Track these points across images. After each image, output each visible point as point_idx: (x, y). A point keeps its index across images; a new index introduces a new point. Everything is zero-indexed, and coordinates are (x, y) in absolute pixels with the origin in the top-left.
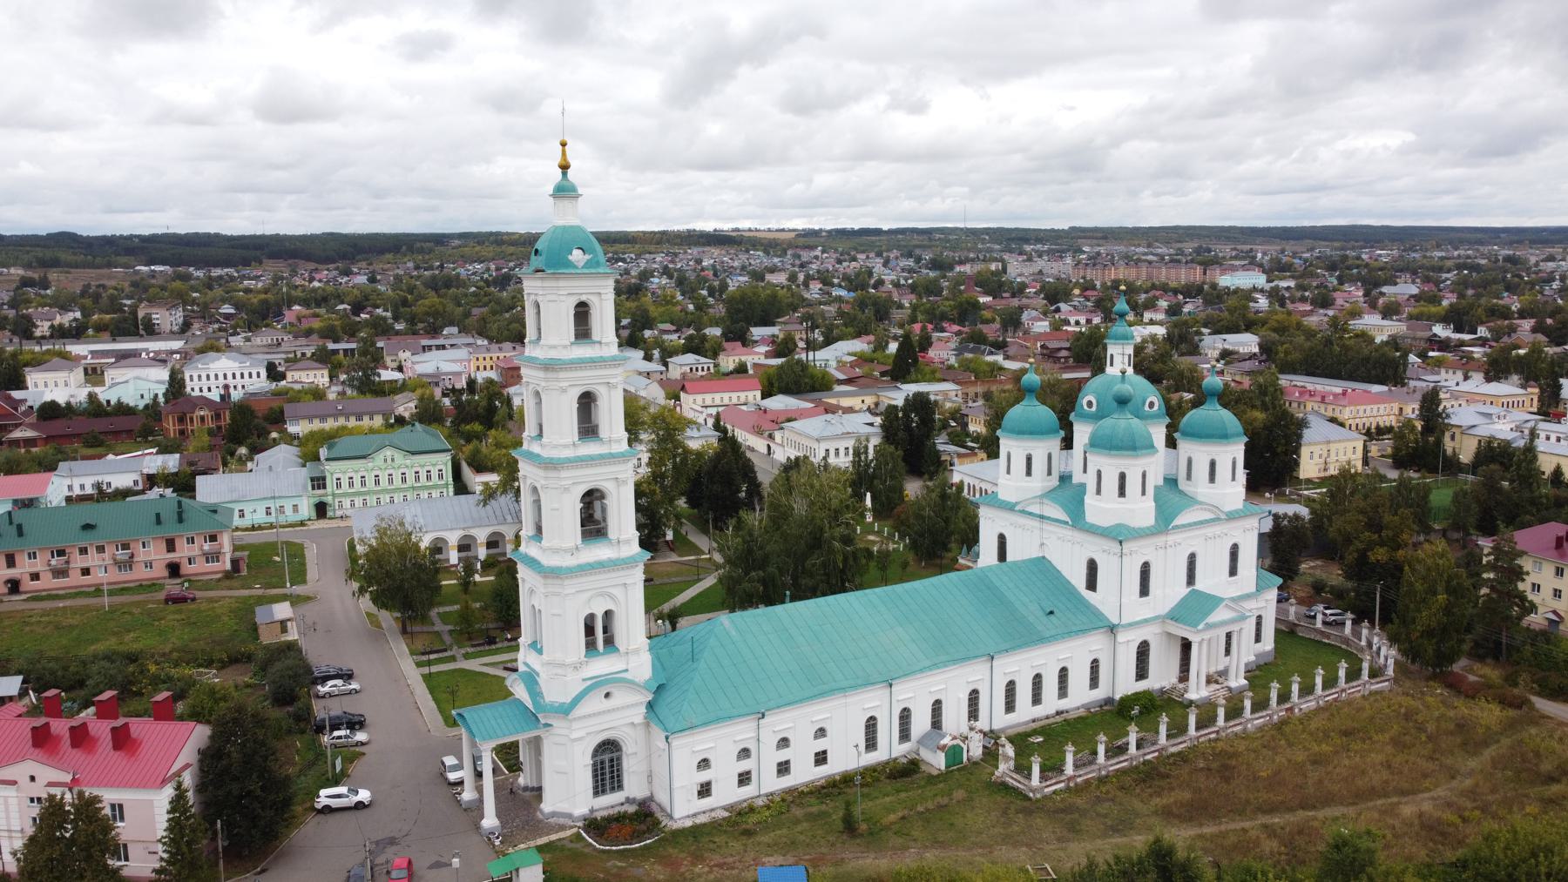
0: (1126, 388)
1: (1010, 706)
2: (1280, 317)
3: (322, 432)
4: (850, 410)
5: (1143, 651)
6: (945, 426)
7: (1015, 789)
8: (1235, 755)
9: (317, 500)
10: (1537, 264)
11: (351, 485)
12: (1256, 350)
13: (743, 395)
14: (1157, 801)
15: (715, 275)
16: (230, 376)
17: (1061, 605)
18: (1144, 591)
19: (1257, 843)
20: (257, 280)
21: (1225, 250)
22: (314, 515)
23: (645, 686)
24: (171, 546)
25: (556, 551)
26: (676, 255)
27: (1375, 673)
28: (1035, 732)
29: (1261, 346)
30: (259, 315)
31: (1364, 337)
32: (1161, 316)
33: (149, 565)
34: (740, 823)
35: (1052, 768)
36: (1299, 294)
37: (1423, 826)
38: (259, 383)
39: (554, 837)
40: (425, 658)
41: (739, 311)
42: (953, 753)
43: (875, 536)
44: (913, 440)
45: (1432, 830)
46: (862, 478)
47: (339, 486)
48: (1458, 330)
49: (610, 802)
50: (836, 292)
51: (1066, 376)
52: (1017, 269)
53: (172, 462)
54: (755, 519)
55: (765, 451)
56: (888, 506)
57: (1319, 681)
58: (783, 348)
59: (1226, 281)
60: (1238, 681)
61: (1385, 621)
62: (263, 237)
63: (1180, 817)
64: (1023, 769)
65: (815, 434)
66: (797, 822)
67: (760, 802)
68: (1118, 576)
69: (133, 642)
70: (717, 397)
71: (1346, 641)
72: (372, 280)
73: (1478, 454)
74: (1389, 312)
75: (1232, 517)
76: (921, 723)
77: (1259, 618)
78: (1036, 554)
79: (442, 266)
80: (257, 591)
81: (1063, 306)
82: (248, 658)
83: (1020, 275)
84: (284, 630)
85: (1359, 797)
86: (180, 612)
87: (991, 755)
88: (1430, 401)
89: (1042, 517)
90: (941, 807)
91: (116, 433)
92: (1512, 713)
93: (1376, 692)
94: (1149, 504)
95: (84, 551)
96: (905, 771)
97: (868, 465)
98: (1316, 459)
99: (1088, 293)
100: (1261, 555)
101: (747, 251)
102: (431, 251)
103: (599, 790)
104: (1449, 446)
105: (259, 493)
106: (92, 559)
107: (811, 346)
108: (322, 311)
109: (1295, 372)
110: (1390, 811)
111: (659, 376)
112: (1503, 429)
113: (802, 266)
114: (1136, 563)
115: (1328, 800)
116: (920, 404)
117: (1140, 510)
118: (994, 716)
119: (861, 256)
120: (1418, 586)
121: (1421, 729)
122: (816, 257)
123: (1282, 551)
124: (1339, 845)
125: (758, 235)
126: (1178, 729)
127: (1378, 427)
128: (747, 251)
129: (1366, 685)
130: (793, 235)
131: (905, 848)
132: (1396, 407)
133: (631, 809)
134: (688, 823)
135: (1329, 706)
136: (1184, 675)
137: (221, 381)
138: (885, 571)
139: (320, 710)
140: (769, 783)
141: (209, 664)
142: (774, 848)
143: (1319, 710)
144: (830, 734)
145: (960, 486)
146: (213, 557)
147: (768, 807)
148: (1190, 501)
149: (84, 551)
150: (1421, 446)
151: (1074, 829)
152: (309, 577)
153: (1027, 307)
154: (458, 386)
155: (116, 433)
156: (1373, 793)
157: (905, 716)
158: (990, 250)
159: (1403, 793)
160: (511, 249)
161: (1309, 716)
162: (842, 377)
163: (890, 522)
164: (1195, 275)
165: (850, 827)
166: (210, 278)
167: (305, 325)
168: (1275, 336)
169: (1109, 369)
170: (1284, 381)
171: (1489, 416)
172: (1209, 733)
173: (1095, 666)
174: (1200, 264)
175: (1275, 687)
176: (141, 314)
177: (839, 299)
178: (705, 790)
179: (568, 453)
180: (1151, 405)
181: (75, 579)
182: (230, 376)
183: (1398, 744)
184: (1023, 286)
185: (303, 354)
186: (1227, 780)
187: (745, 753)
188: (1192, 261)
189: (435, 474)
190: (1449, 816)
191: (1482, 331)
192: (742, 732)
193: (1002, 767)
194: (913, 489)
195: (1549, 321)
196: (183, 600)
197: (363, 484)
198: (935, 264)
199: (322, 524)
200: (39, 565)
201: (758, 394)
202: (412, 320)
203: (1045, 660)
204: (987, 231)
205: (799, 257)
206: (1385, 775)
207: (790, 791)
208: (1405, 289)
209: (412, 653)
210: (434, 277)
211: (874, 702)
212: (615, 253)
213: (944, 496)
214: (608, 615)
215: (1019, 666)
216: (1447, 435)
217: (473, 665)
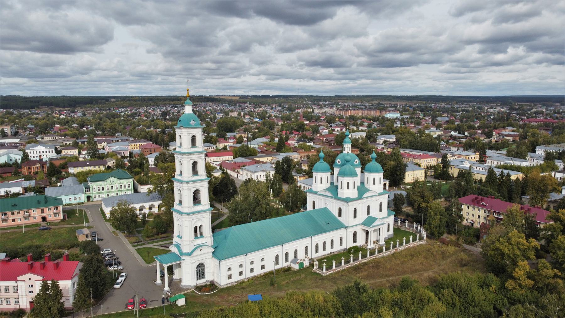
0: (348, 158)
1: (317, 251)
2: (403, 129)
3: (83, 172)
4: (263, 162)
5: (355, 234)
6: (294, 167)
7: (319, 274)
8: (379, 262)
9: (87, 195)
10: (487, 110)
12: (395, 140)
15: (211, 113)
16: (41, 152)
18: (355, 217)
20: (39, 114)
21: (387, 104)
22: (86, 200)
23: (212, 247)
24: (43, 211)
26: (196, 105)
27: (421, 239)
28: (324, 258)
29: (396, 139)
30: (45, 129)
31: (429, 136)
32: (365, 128)
34: (240, 286)
35: (329, 267)
36: (410, 120)
38: (53, 155)
39: (186, 292)
41: (222, 127)
43: (276, 204)
44: (285, 171)
46: (270, 184)
47: (95, 190)
48: (459, 133)
49: (201, 282)
51: (333, 150)
52: (318, 111)
53: (32, 183)
54: (238, 198)
55: (236, 176)
56: (277, 194)
57: (404, 241)
58: (240, 141)
59: (388, 116)
60: (382, 242)
62: (37, 97)
64: (321, 268)
66: (257, 285)
68: (348, 210)
69: (36, 242)
70: (218, 158)
72: (84, 115)
73: (459, 174)
74: (438, 127)
75: (380, 194)
76: (291, 257)
77: (389, 224)
79: (109, 109)
80: (73, 225)
81: (333, 125)
86: (49, 232)
87: (312, 265)
88: (444, 157)
89: (325, 196)
90: (298, 279)
92: (457, 248)
94: (356, 191)
96: (288, 270)
97: (271, 180)
98: (410, 176)
100: (389, 206)
101: (222, 104)
102: (104, 103)
103: (198, 278)
104: (450, 171)
106: (16, 216)
107: (249, 140)
108: (67, 127)
109: (406, 148)
113: (242, 110)
114: (354, 210)
116: (287, 161)
117: (353, 193)
118: (312, 254)
120: (432, 213)
122: (247, 106)
123: (396, 206)
125: (226, 97)
126: (364, 256)
127: (430, 166)
128: (222, 104)
129: (418, 243)
133: (208, 283)
134: (225, 286)
135: (407, 248)
136: (367, 242)
137: (38, 154)
138: (278, 213)
140: (248, 275)
142: (250, 292)
144: (266, 260)
145: (300, 187)
147: (248, 281)
148: (368, 190)
149: (13, 214)
152: (90, 220)
153: (321, 125)
154: (126, 155)
157: (287, 254)
158: (308, 104)
159: (425, 270)
160: (135, 103)
161: (402, 251)
162: (260, 151)
163: (279, 198)
164: (377, 113)
166: (20, 114)
167: (62, 133)
168: (401, 136)
169: (344, 152)
170: (402, 151)
172: (373, 257)
174: (379, 109)
177: (257, 122)
179: (190, 179)
180: (356, 162)
182: (41, 152)
183: (426, 258)
184: (319, 117)
185: (66, 144)
186: (378, 269)
188: (376, 108)
189: (127, 186)
191: (466, 134)
192: (240, 259)
193: (315, 267)
194: (285, 188)
195: (486, 130)
197: (103, 189)
198: (290, 109)
199: (89, 203)
201: (232, 157)
202: (103, 131)
204: (307, 96)
205: (241, 106)
208: (444, 118)
209: (131, 243)
210: (108, 114)
212: (174, 104)
213: (295, 190)
215: (319, 239)
216: (450, 168)
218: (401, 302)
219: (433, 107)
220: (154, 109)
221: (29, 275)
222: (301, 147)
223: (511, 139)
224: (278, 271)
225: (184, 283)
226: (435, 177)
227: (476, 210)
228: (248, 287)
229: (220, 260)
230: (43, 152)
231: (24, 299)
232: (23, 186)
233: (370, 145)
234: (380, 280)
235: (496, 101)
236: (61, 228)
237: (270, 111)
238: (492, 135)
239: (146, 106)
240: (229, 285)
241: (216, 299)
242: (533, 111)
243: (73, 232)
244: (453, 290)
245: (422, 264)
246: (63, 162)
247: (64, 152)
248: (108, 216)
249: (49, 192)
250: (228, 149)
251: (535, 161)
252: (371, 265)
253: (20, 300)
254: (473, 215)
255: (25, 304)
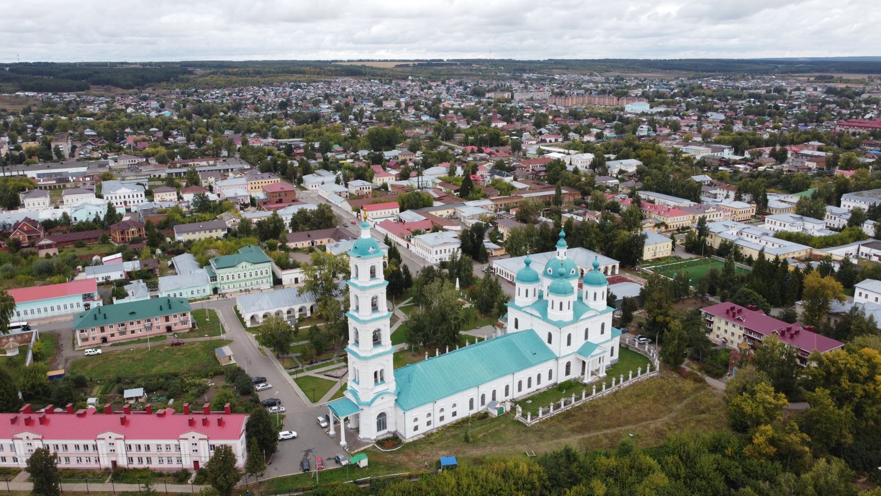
1: (520, 390)
5: (568, 366)
8: (598, 406)
10: (790, 93)
11: (228, 279)
13: (391, 211)
14: (570, 426)
15: (355, 100)
17: (540, 350)
18: (569, 344)
19: (601, 440)
24: (167, 319)
25: (365, 351)
26: (329, 83)
27: (652, 369)
30: (112, 140)
33: (158, 327)
34: (429, 439)
35: (535, 415)
37: (656, 432)
38: (145, 203)
40: (293, 370)
42: (500, 410)
44: (473, 244)
45: (660, 434)
47: (223, 279)
48: (736, 153)
49: (383, 434)
50: (425, 118)
53: (134, 265)
56: (468, 281)
57: (630, 375)
60: (602, 374)
61: (660, 342)
63: (577, 432)
64: (524, 415)
65: (431, 244)
66: (449, 438)
67: (434, 431)
68: (559, 338)
71: (646, 353)
74: (706, 140)
75: (602, 313)
76: (488, 399)
78: (529, 328)
79: (196, 91)
80: (207, 338)
81: (543, 130)
82: (222, 373)
83: (521, 101)
84: (230, 359)
85: (638, 421)
86: (180, 350)
87: (513, 409)
88: (702, 221)
91: (89, 239)
92: (698, 385)
93: (652, 377)
94: (571, 312)
95: (132, 323)
96: (483, 417)
99: (557, 119)
103: (379, 429)
104: (708, 239)
105: (186, 281)
106: (135, 327)
110: (647, 427)
111: (344, 195)
112: (730, 234)
113: (402, 92)
114: (564, 325)
115: (627, 423)
117: (568, 315)
118: (515, 394)
119: (434, 84)
121: (664, 393)
122: (409, 86)
124: (623, 444)
128: (370, 80)
129: (649, 374)
130: (393, 65)
131: (486, 447)
132: (691, 216)
133: (391, 435)
136: (583, 374)
137: (123, 200)
139: (263, 397)
140: (437, 424)
141: (206, 376)
142: (442, 448)
143: (630, 386)
144: (458, 406)
146: (184, 322)
148: (587, 308)
150: (696, 243)
151: (542, 438)
155: (89, 239)
156: (643, 420)
157: (483, 397)
159: (653, 419)
160: (234, 78)
161: (626, 389)
162: (436, 196)
163: (467, 291)
165: (467, 439)
171: (727, 227)
172: (590, 398)
173: (550, 372)
175: (614, 379)
176: (53, 145)
177: (425, 123)
178: (416, 428)
181: (129, 335)
183: (655, 400)
186: (594, 417)
187: (429, 415)
189: (264, 272)
190: (665, 428)
191: (747, 155)
192: (428, 408)
196: (178, 344)
197: (233, 278)
198: (478, 93)
200: (114, 330)
201: (398, 210)
203: (532, 372)
205: (399, 85)
206: (648, 413)
207: (444, 426)
209: (286, 368)
211: (474, 393)
212: (295, 81)
214: (382, 371)
217: (311, 373)
218: (618, 472)
219: (703, 85)
220: (265, 92)
221: (193, 434)
222: (495, 185)
223: (813, 165)
224: (474, 417)
225: (362, 435)
226: (688, 250)
227: (730, 325)
228: (438, 440)
229: (405, 411)
230: (127, 196)
231: (188, 459)
232: (126, 270)
233: (599, 180)
234: (595, 434)
235: (808, 72)
236: (194, 343)
237: (444, 95)
238: (786, 157)
239: (253, 85)
240: (415, 438)
241: (402, 458)
242: (865, 96)
243: (211, 348)
244: (680, 457)
245: (649, 409)
246: (162, 218)
247: (157, 197)
248: (249, 324)
249: (167, 286)
250: (390, 189)
251: (837, 219)
252: (586, 410)
253: (183, 459)
254: (726, 331)
255: (189, 463)
